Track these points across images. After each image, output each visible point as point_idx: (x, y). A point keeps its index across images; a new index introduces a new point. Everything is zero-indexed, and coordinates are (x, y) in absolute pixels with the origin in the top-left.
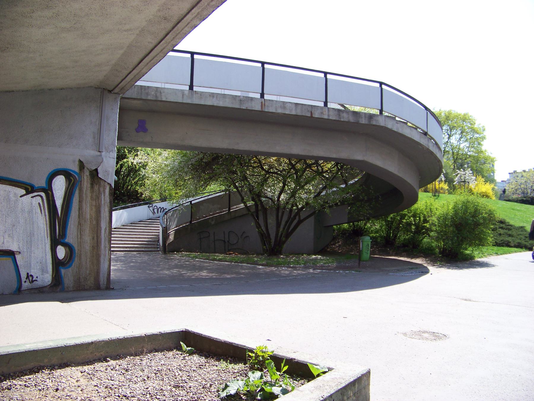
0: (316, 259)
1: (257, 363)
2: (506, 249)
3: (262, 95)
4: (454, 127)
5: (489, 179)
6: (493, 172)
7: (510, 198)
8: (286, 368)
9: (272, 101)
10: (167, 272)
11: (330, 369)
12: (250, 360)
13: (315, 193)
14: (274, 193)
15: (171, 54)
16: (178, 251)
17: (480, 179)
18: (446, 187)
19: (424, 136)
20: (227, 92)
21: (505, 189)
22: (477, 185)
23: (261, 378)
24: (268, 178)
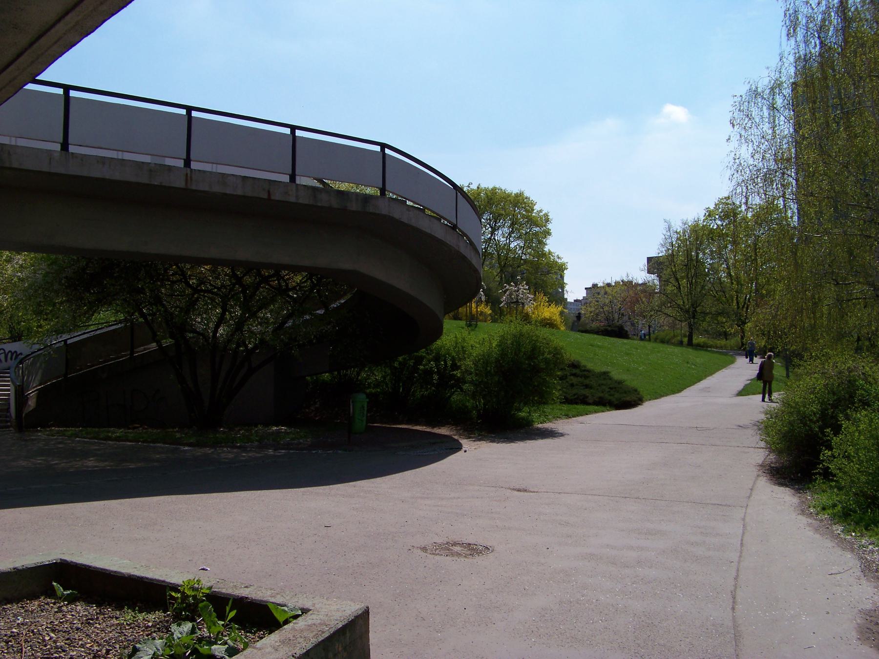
0: (278, 432)
1: (184, 609)
2: (581, 407)
3: (187, 162)
4: (500, 215)
5: (557, 298)
6: (563, 288)
7: (588, 327)
8: (232, 614)
9: (204, 172)
10: (24, 463)
11: (305, 611)
12: (173, 604)
13: (274, 323)
14: (207, 325)
15: (31, 87)
16: (44, 426)
17: (541, 297)
18: (488, 311)
19: (452, 231)
20: (127, 156)
21: (579, 314)
22: (536, 308)
23: (193, 631)
24: (197, 299)
